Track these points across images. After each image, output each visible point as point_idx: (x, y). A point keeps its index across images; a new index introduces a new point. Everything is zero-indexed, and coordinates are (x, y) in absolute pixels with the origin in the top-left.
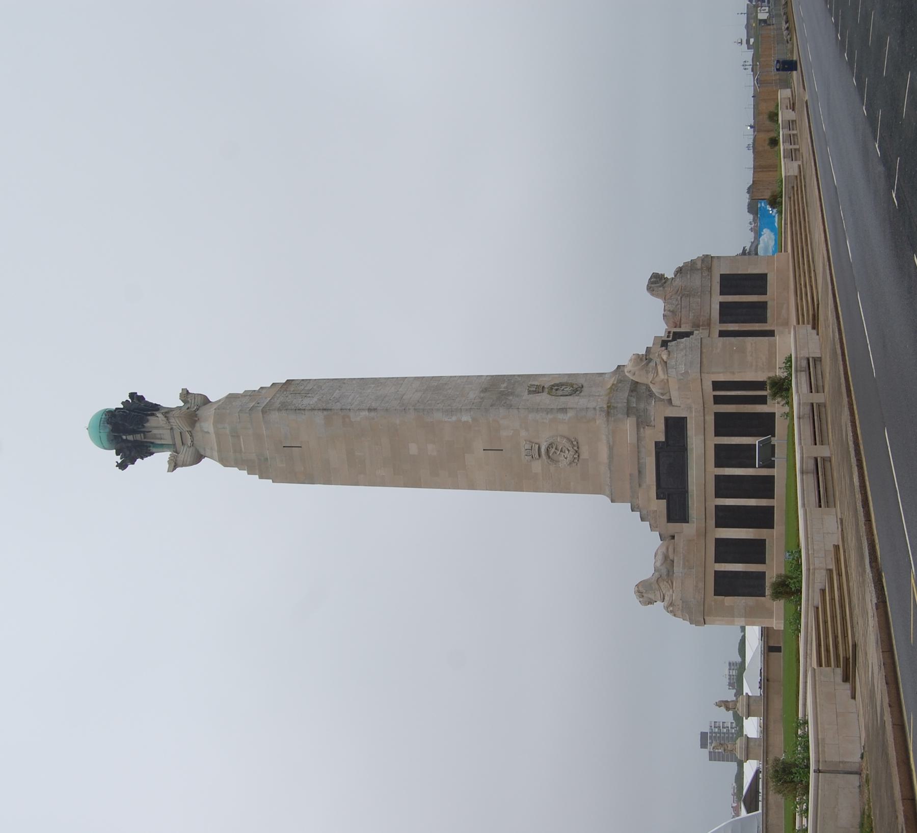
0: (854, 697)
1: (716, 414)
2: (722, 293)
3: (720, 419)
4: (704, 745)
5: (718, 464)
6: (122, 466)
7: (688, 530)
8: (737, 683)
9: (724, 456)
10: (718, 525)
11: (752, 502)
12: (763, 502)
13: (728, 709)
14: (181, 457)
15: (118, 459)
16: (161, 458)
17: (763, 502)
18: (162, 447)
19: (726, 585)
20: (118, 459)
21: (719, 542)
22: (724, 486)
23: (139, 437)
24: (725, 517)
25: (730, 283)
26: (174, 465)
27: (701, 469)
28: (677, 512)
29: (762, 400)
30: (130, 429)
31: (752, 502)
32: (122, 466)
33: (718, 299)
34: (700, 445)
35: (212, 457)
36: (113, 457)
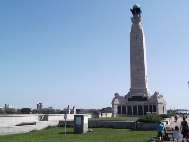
0: (16, 125)
1: (147, 106)
3: (136, 106)
4: (40, 103)
5: (139, 106)
6: (131, 10)
7: (127, 101)
9: (140, 107)
10: (128, 106)
11: (132, 112)
15: (132, 9)
16: (132, 16)
18: (134, 16)
20: (132, 9)
21: (125, 106)
22: (135, 107)
24: (129, 107)
25: (155, 107)
27: (138, 103)
28: (130, 100)
30: (136, 11)
31: (132, 112)
32: (131, 10)
35: (133, 24)
36: (140, 9)
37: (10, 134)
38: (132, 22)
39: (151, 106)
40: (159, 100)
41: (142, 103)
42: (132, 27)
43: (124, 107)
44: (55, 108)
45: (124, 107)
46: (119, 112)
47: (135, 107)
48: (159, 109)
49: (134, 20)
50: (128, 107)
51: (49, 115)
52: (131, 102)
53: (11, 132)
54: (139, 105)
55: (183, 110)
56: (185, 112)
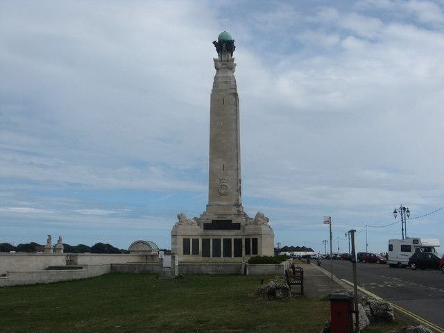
2: (220, 257)
8: (286, 249)
9: (227, 241)
10: (213, 239)
12: (211, 254)
13: (59, 241)
14: (218, 63)
16: (216, 55)
17: (211, 254)
19: (186, 241)
21: (198, 240)
22: (217, 241)
23: (224, 49)
24: (206, 242)
25: (255, 241)
26: (215, 60)
27: (223, 234)
28: (207, 227)
29: (248, 253)
32: (214, 43)
33: (222, 258)
34: (232, 234)
37: (14, 283)
38: (217, 68)
39: (247, 241)
40: (264, 228)
41: (232, 234)
42: (216, 78)
43: (196, 242)
44: (114, 245)
45: (196, 242)
46: (186, 252)
47: (217, 241)
48: (208, 194)
49: (220, 65)
50: (204, 240)
51: (79, 254)
52: (210, 232)
53: (35, 279)
54: (225, 237)
55: (298, 249)
56: (303, 254)
